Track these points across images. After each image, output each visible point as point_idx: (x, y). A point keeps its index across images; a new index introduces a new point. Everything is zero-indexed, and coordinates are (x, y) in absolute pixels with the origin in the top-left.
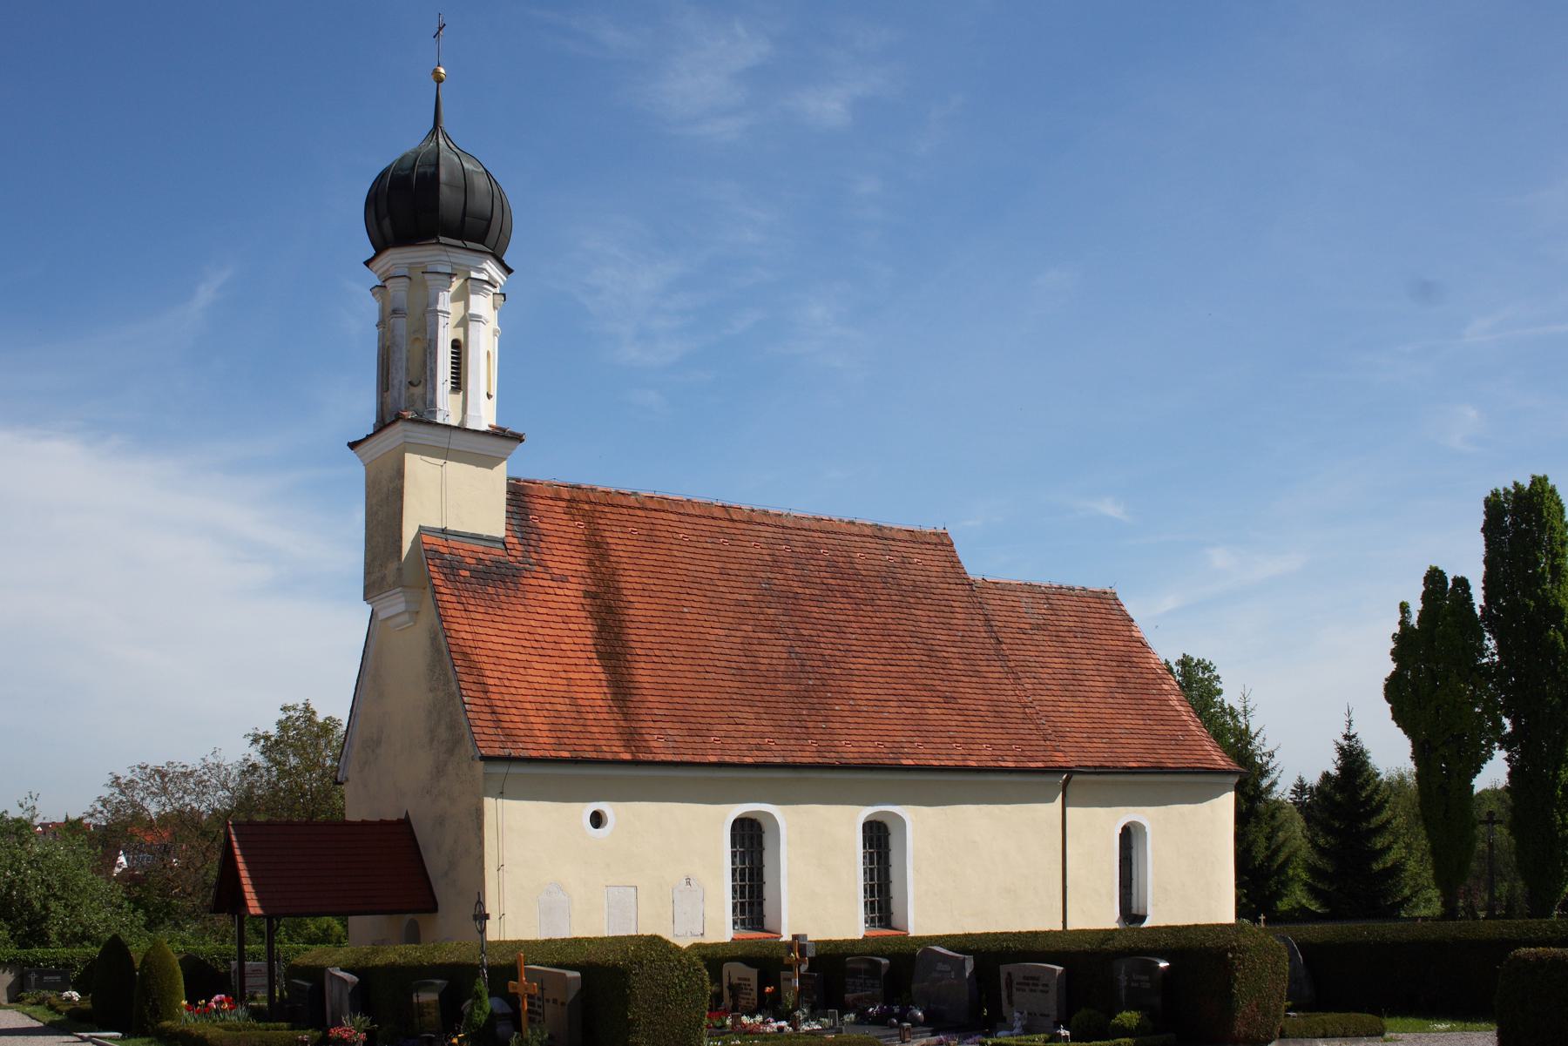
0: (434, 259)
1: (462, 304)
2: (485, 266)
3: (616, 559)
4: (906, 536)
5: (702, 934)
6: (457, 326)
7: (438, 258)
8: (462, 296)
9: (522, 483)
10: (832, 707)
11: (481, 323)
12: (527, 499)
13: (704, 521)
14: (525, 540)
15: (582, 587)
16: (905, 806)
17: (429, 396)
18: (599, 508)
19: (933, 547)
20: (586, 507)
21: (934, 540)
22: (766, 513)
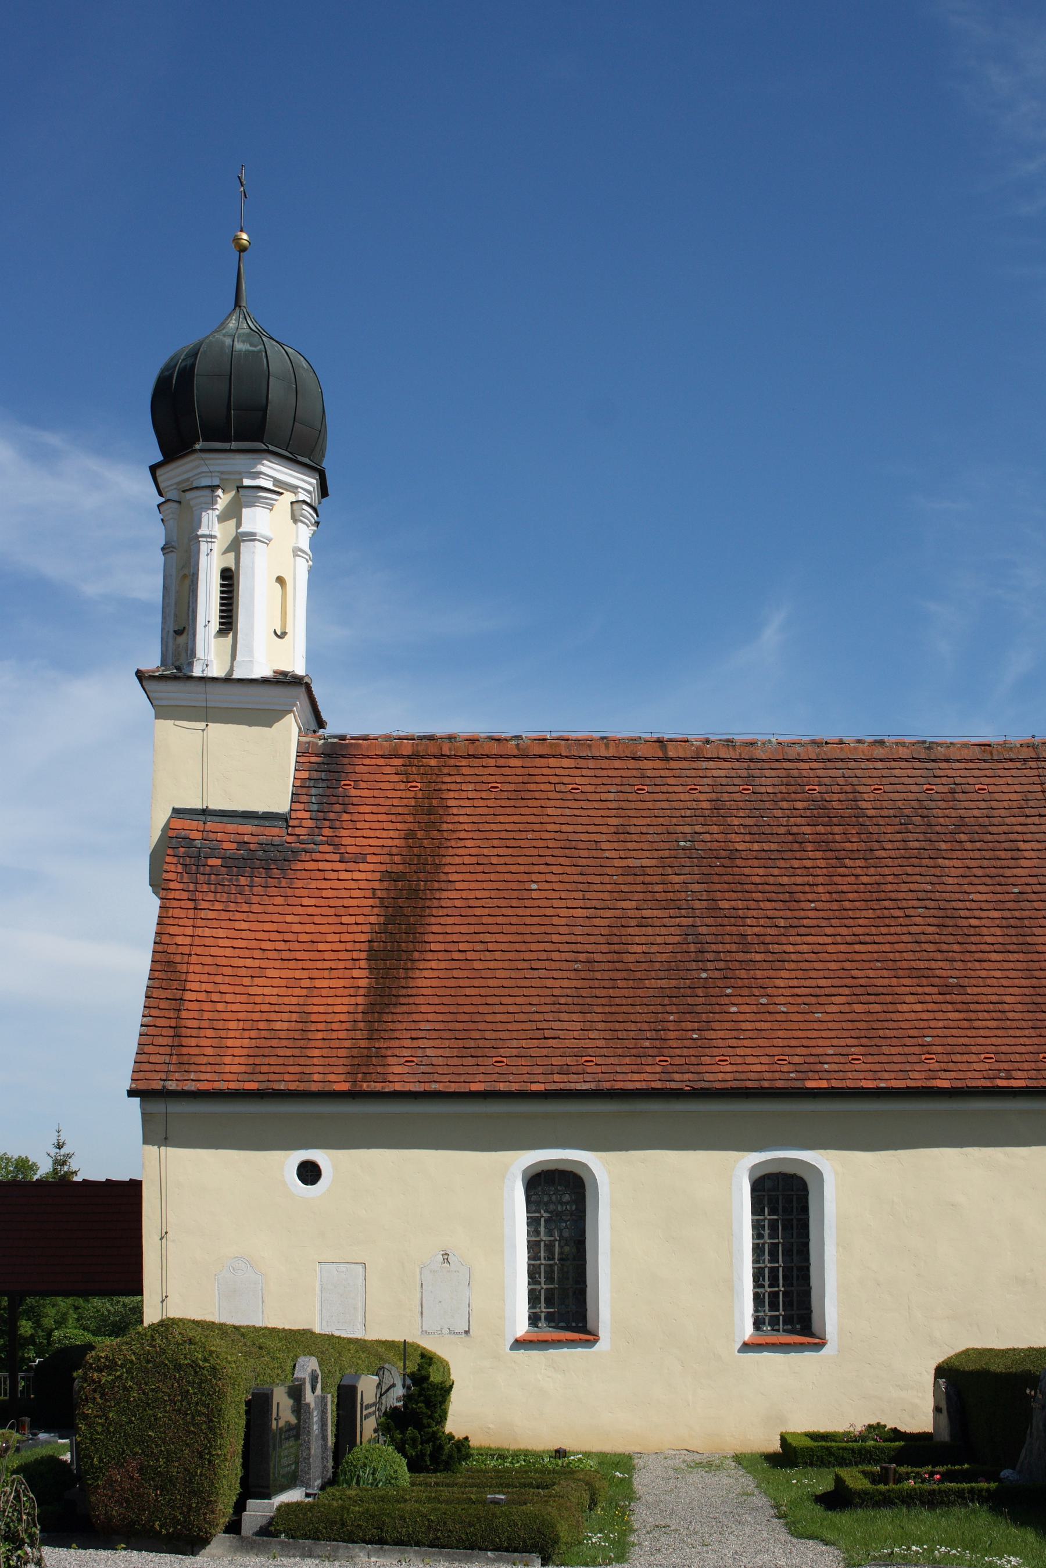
0: (196, 472)
1: (233, 523)
2: (263, 469)
3: (450, 826)
4: (977, 752)
5: (467, 1332)
6: (227, 551)
7: (199, 470)
8: (233, 513)
9: (347, 741)
10: (725, 1008)
11: (257, 542)
12: (346, 761)
13: (617, 764)
14: (321, 816)
15: (383, 868)
16: (822, 1151)
17: (190, 646)
18: (452, 762)
19: (1018, 765)
20: (433, 762)
21: (1026, 753)
22: (729, 743)
